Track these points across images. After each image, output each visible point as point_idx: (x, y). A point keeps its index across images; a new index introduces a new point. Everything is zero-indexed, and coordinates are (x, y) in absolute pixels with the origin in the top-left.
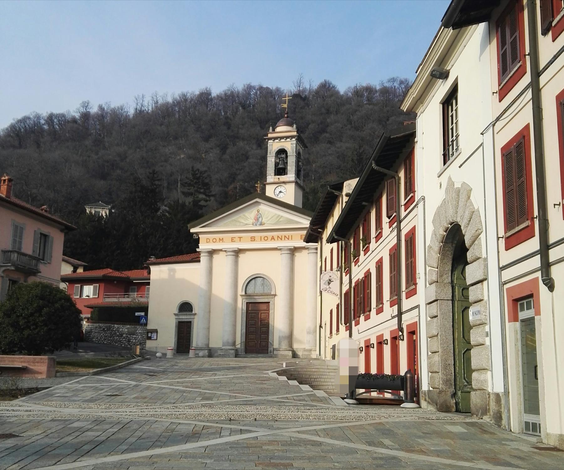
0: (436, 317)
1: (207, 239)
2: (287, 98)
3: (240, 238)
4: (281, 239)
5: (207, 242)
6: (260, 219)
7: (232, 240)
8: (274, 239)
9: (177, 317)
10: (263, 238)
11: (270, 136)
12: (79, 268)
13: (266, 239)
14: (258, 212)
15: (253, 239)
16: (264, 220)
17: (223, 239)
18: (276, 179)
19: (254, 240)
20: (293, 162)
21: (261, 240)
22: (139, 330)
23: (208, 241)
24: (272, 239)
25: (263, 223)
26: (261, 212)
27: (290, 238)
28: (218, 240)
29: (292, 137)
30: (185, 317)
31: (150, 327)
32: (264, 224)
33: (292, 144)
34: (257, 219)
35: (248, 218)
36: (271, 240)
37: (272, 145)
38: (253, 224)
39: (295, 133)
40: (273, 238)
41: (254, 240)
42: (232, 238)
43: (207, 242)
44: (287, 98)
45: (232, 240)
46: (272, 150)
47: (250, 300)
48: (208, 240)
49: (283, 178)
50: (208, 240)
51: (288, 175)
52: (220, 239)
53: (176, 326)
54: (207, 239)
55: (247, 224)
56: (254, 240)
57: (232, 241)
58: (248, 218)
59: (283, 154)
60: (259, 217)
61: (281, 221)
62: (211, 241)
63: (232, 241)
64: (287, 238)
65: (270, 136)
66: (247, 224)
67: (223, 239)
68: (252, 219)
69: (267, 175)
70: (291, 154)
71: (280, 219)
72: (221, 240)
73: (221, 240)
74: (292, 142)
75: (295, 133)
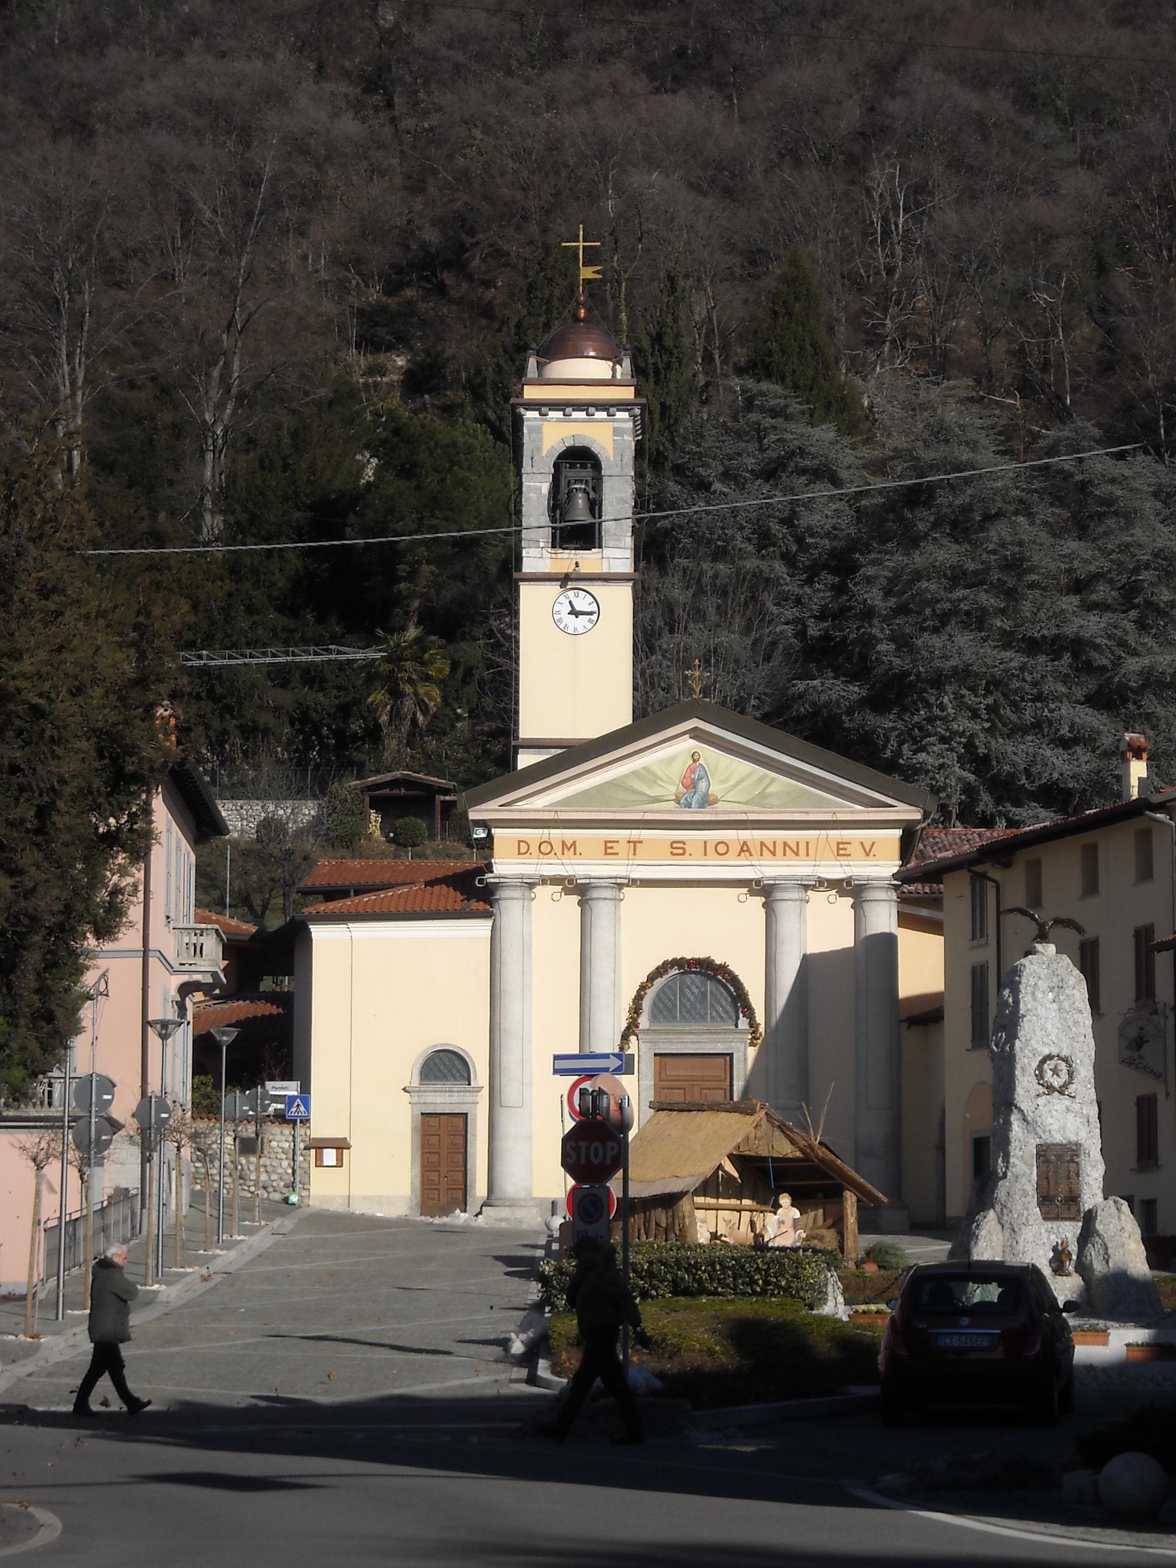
0: (47, 1362)
1: (519, 842)
2: (581, 244)
3: (635, 843)
4: (774, 854)
5: (519, 853)
6: (702, 785)
7: (606, 847)
8: (748, 850)
9: (415, 1100)
10: (710, 849)
11: (531, 393)
12: (248, 938)
13: (722, 849)
14: (694, 761)
15: (678, 850)
16: (715, 789)
17: (574, 843)
18: (567, 560)
19: (683, 854)
20: (622, 501)
21: (705, 854)
22: (278, 1138)
23: (522, 848)
24: (742, 850)
25: (711, 798)
26: (706, 760)
27: (802, 851)
28: (558, 848)
29: (622, 405)
30: (443, 1099)
31: (320, 1128)
32: (716, 801)
33: (616, 432)
34: (691, 784)
35: (661, 780)
36: (739, 855)
37: (539, 430)
38: (678, 801)
39: (628, 393)
40: (744, 848)
41: (681, 851)
42: (606, 842)
43: (519, 853)
44: (581, 244)
45: (608, 849)
46: (539, 449)
47: (668, 1045)
48: (524, 848)
49: (589, 561)
50: (524, 848)
51: (607, 552)
52: (564, 843)
53: (414, 1130)
54: (519, 842)
55: (656, 800)
56: (681, 851)
57: (606, 854)
58: (661, 780)
59: (583, 466)
60: (700, 779)
61: (772, 794)
62: (534, 849)
63: (606, 854)
64: (790, 847)
65: (531, 393)
66: (656, 800)
67: (574, 843)
68: (673, 783)
69: (524, 544)
70: (615, 471)
71: (768, 786)
72: (569, 849)
73: (570, 847)
74: (616, 425)
75: (628, 393)
